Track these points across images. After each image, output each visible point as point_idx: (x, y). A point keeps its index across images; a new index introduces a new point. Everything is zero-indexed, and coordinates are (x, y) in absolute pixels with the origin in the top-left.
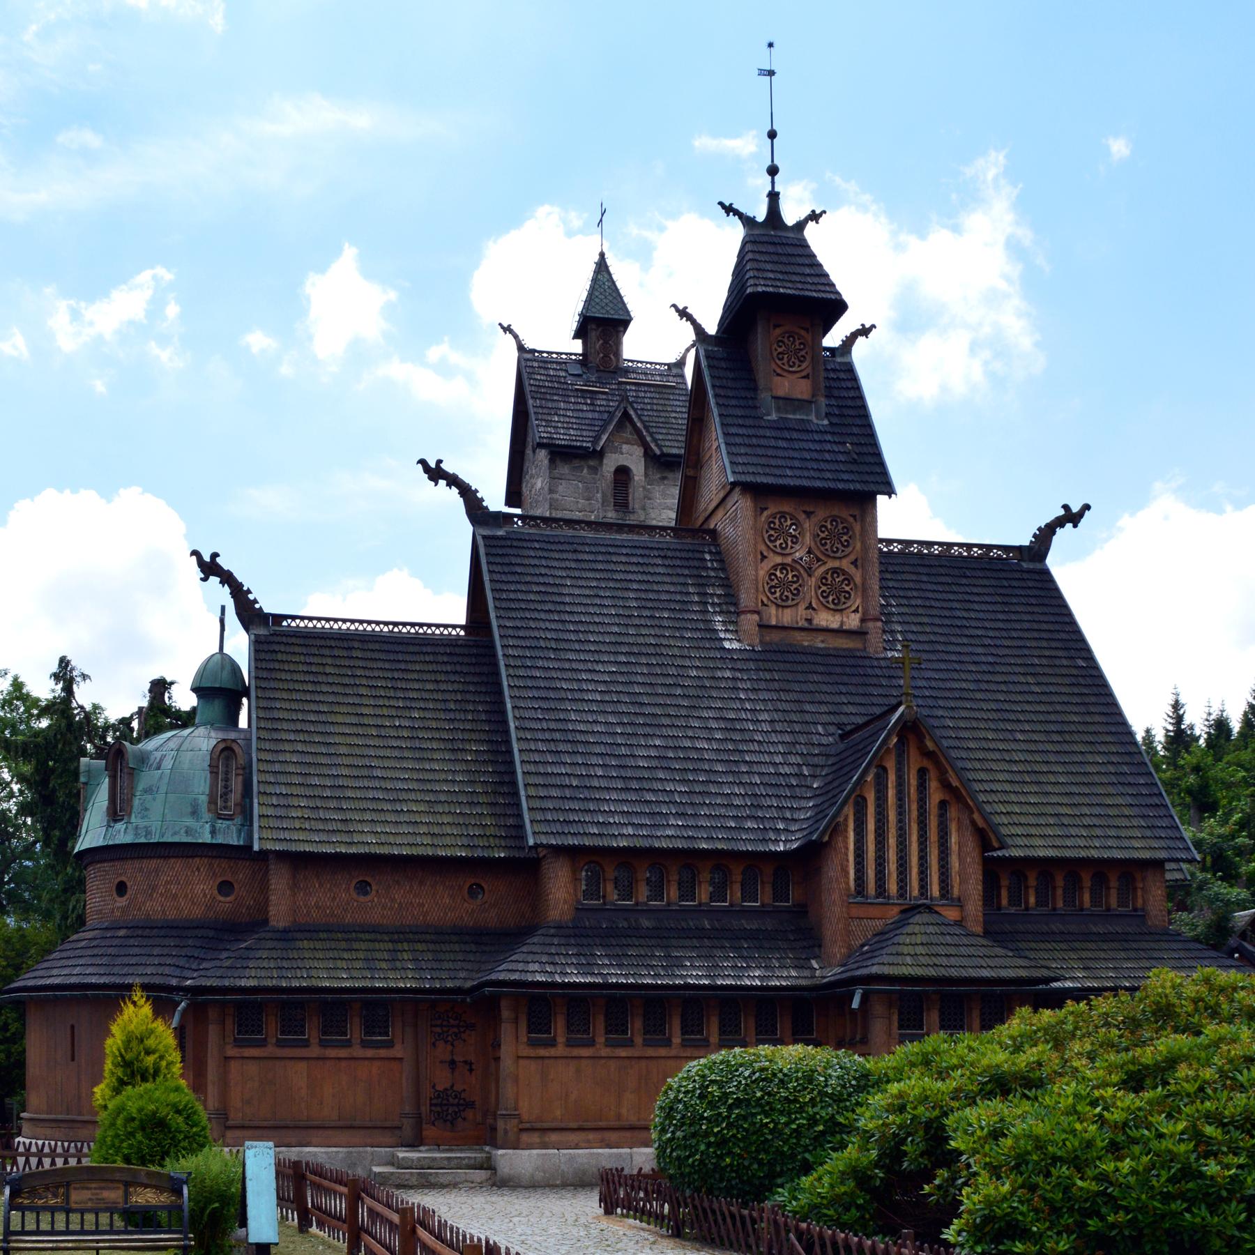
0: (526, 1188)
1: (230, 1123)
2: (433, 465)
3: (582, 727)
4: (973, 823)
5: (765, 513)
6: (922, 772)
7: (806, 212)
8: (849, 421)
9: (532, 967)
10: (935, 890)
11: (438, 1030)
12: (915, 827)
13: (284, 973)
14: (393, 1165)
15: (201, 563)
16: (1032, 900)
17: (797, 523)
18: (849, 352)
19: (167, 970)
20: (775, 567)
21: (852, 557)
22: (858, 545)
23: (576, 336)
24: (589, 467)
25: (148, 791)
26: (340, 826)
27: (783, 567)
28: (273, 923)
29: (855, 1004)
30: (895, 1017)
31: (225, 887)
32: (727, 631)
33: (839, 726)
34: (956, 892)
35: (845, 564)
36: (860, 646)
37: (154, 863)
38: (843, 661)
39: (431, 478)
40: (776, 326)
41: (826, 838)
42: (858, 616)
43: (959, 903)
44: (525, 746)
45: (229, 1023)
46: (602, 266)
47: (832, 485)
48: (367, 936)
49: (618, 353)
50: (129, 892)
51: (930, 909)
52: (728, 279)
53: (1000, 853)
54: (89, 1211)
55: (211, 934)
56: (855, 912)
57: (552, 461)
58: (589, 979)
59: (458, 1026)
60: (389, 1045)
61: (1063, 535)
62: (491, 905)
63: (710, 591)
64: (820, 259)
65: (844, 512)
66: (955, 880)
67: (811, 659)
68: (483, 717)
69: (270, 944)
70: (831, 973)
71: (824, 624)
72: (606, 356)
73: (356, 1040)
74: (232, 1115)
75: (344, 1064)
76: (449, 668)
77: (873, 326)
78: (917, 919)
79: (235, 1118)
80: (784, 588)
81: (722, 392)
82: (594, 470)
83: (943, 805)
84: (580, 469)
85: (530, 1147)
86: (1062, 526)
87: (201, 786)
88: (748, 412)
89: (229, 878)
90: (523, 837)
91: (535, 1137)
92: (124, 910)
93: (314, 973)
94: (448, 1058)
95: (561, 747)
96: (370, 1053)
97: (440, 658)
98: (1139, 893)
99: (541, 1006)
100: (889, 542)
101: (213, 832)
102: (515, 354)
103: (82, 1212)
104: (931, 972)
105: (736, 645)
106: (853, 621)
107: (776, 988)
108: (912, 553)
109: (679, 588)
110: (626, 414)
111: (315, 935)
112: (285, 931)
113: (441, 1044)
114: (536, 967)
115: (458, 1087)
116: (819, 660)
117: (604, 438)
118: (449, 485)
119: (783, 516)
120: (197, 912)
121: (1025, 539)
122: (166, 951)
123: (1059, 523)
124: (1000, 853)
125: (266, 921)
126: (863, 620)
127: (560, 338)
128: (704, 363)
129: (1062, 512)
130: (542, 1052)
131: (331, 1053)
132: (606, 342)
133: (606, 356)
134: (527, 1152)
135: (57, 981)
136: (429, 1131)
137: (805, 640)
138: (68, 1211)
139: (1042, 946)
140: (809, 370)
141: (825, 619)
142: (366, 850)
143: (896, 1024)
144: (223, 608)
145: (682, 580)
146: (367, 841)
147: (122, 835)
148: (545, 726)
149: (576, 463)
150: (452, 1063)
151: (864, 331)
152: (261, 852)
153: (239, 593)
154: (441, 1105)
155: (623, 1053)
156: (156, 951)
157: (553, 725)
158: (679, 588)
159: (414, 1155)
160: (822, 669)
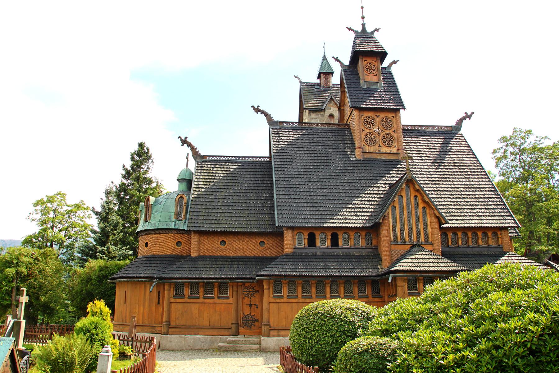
1: (170, 326)
3: (299, 186)
4: (435, 214)
6: (416, 197)
9: (274, 269)
10: (423, 239)
11: (246, 293)
12: (414, 217)
15: (182, 140)
16: (460, 243)
19: (154, 272)
21: (393, 130)
22: (395, 126)
26: (216, 222)
27: (370, 133)
29: (390, 280)
30: (406, 286)
31: (179, 243)
33: (389, 184)
34: (430, 240)
36: (397, 158)
41: (381, 221)
43: (432, 244)
44: (278, 193)
45: (172, 289)
48: (223, 260)
53: (447, 225)
55: (172, 259)
56: (393, 247)
58: (295, 274)
59: (253, 292)
60: (228, 298)
61: (466, 122)
62: (267, 248)
63: (347, 142)
65: (390, 115)
66: (430, 235)
67: (380, 163)
71: (385, 151)
73: (285, 296)
74: (172, 323)
75: (211, 305)
76: (259, 170)
79: (173, 324)
80: (370, 140)
81: (348, 81)
82: (322, 115)
83: (424, 208)
84: (318, 115)
85: (274, 336)
86: (465, 119)
87: (172, 210)
88: (356, 86)
90: (275, 225)
91: (275, 333)
92: (147, 251)
93: (201, 272)
95: (291, 193)
96: (221, 301)
97: (257, 167)
98: (500, 239)
99: (277, 282)
101: (175, 225)
102: (299, 84)
105: (354, 159)
106: (395, 150)
109: (336, 142)
110: (331, 98)
111: (205, 259)
113: (246, 298)
114: (276, 269)
115: (253, 314)
116: (383, 163)
117: (325, 105)
119: (369, 117)
120: (169, 253)
121: (453, 124)
122: (156, 265)
123: (464, 118)
124: (447, 225)
126: (398, 150)
127: (313, 78)
128: (343, 73)
129: (465, 115)
130: (278, 301)
131: (207, 301)
135: (120, 276)
136: (241, 330)
137: (378, 157)
139: (464, 259)
140: (377, 73)
141: (385, 149)
144: (188, 154)
145: (337, 139)
146: (224, 226)
147: (147, 227)
148: (286, 186)
149: (317, 113)
151: (395, 62)
152: (187, 230)
153: (193, 149)
154: (246, 320)
156: (153, 265)
157: (289, 186)
158: (336, 142)
160: (384, 166)
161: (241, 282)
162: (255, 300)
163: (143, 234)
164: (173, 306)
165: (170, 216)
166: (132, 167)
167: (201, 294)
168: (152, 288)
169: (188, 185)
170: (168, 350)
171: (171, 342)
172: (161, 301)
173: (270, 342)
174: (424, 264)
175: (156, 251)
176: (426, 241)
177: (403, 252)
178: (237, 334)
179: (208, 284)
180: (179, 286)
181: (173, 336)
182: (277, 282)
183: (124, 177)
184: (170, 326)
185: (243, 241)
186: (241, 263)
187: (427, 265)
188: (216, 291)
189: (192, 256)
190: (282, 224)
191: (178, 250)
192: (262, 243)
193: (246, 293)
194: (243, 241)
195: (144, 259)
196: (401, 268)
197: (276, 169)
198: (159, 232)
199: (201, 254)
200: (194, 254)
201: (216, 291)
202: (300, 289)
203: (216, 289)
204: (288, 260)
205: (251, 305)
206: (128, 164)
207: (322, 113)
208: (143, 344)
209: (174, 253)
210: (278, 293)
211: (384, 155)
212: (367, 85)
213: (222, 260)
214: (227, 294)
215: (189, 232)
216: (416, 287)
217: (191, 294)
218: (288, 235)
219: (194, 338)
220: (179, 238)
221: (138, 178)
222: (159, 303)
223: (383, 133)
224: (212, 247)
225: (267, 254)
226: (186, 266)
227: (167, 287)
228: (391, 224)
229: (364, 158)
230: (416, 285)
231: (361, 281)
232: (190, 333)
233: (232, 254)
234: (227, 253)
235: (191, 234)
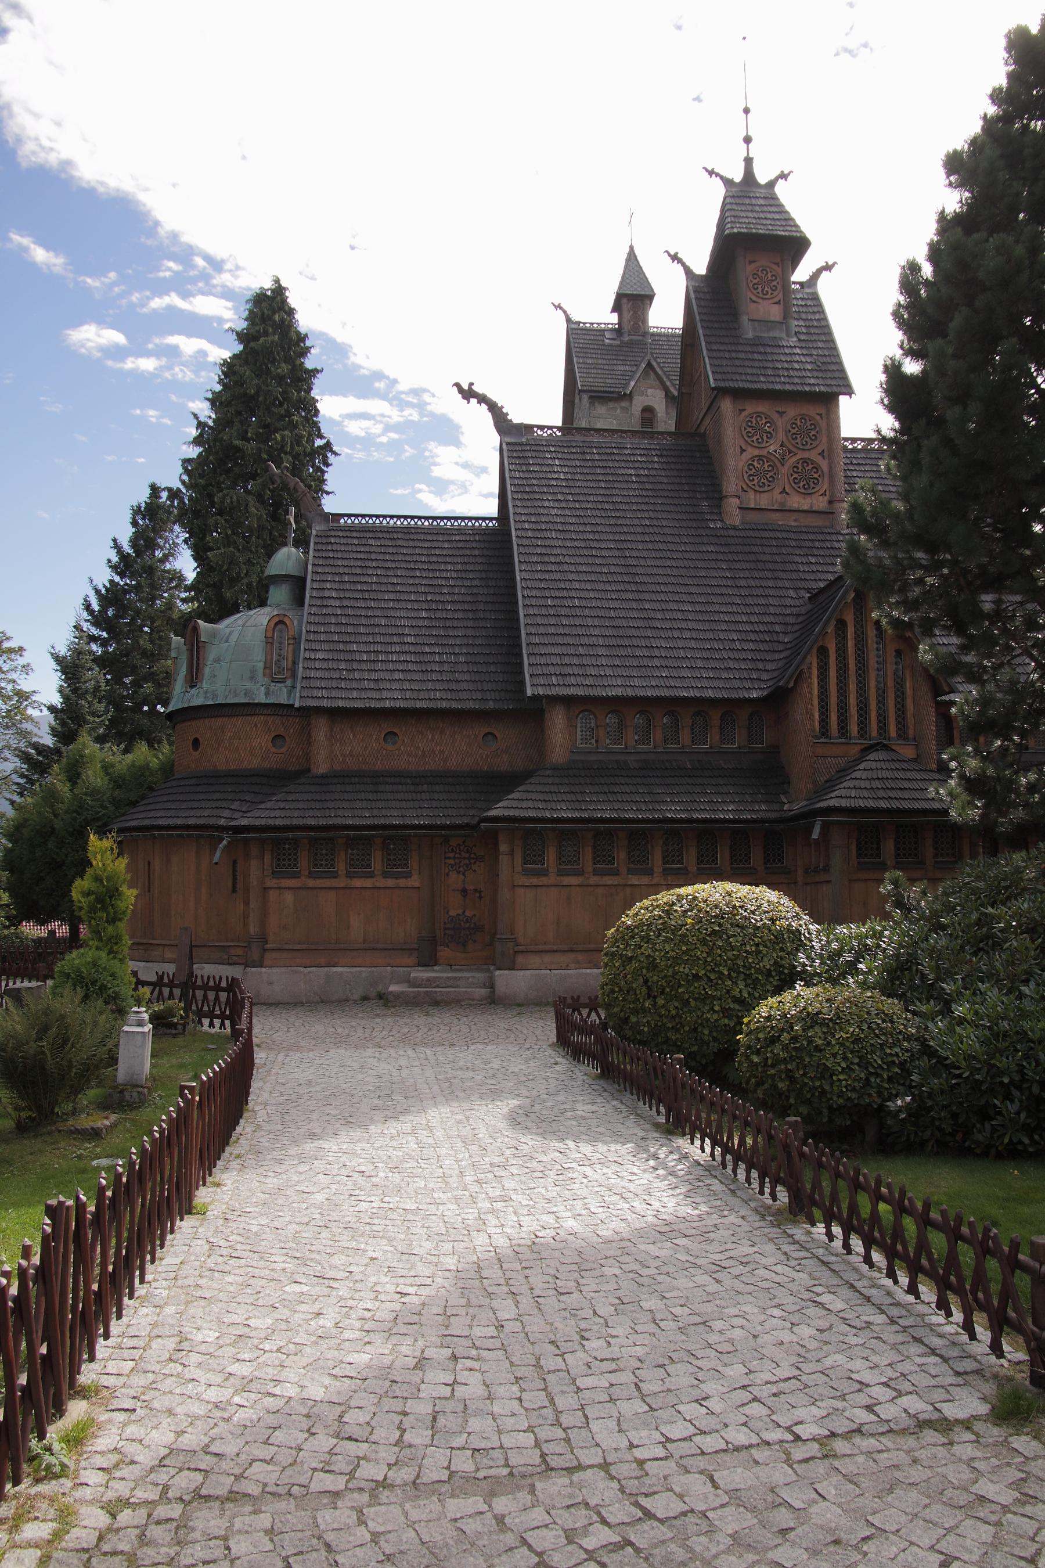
1: (268, 946)
2: (466, 387)
5: (744, 414)
7: (777, 173)
8: (815, 337)
10: (893, 733)
11: (452, 862)
17: (771, 422)
18: (815, 284)
20: (753, 459)
22: (825, 439)
23: (613, 311)
24: (622, 408)
25: (217, 660)
27: (760, 458)
28: (314, 771)
30: (854, 847)
32: (712, 513)
33: (808, 590)
34: (911, 733)
35: (813, 455)
37: (220, 721)
38: (813, 537)
39: (464, 398)
40: (751, 262)
42: (826, 498)
46: (632, 258)
47: (800, 388)
48: (392, 780)
49: (645, 321)
50: (201, 747)
51: (886, 748)
52: (714, 230)
57: (592, 404)
58: (577, 815)
59: (469, 858)
60: (408, 875)
62: (503, 749)
64: (788, 208)
65: (812, 410)
70: (797, 807)
71: (796, 506)
72: (636, 323)
77: (835, 263)
78: (871, 757)
80: (762, 473)
82: (625, 410)
89: (281, 731)
90: (524, 691)
96: (390, 882)
99: (532, 833)
100: (854, 440)
101: (267, 694)
104: (883, 804)
106: (820, 503)
107: (747, 821)
108: (873, 450)
112: (323, 776)
113: (453, 875)
117: (632, 383)
118: (479, 402)
119: (759, 415)
120: (255, 763)
125: (309, 770)
126: (830, 502)
128: (693, 296)
130: (535, 881)
131: (357, 883)
132: (635, 313)
133: (636, 323)
134: (522, 973)
136: (444, 953)
141: (796, 501)
142: (393, 704)
143: (854, 852)
146: (393, 698)
149: (611, 405)
150: (464, 892)
151: (828, 267)
152: (301, 708)
155: (609, 880)
161: (435, 838)
164: (272, 895)
166: (134, 542)
167: (341, 866)
168: (218, 853)
170: (264, 1004)
171: (270, 983)
172: (240, 885)
173: (513, 981)
174: (900, 794)
176: (899, 736)
177: (842, 762)
178: (428, 961)
181: (275, 970)
183: (114, 568)
184: (268, 946)
187: (906, 795)
188: (377, 862)
190: (541, 691)
192: (490, 737)
193: (452, 862)
195: (192, 781)
196: (844, 803)
197: (522, 550)
199: (337, 767)
200: (321, 767)
202: (588, 854)
203: (379, 853)
204: (557, 780)
205: (464, 892)
206: (125, 534)
207: (624, 404)
208: (211, 995)
209: (266, 765)
210: (534, 863)
211: (795, 516)
212: (754, 329)
213: (389, 780)
214: (406, 865)
215: (307, 713)
216: (878, 849)
217: (315, 865)
218: (557, 721)
221: (150, 570)
222: (234, 890)
223: (794, 459)
228: (816, 692)
229: (742, 523)
230: (878, 843)
231: (738, 833)
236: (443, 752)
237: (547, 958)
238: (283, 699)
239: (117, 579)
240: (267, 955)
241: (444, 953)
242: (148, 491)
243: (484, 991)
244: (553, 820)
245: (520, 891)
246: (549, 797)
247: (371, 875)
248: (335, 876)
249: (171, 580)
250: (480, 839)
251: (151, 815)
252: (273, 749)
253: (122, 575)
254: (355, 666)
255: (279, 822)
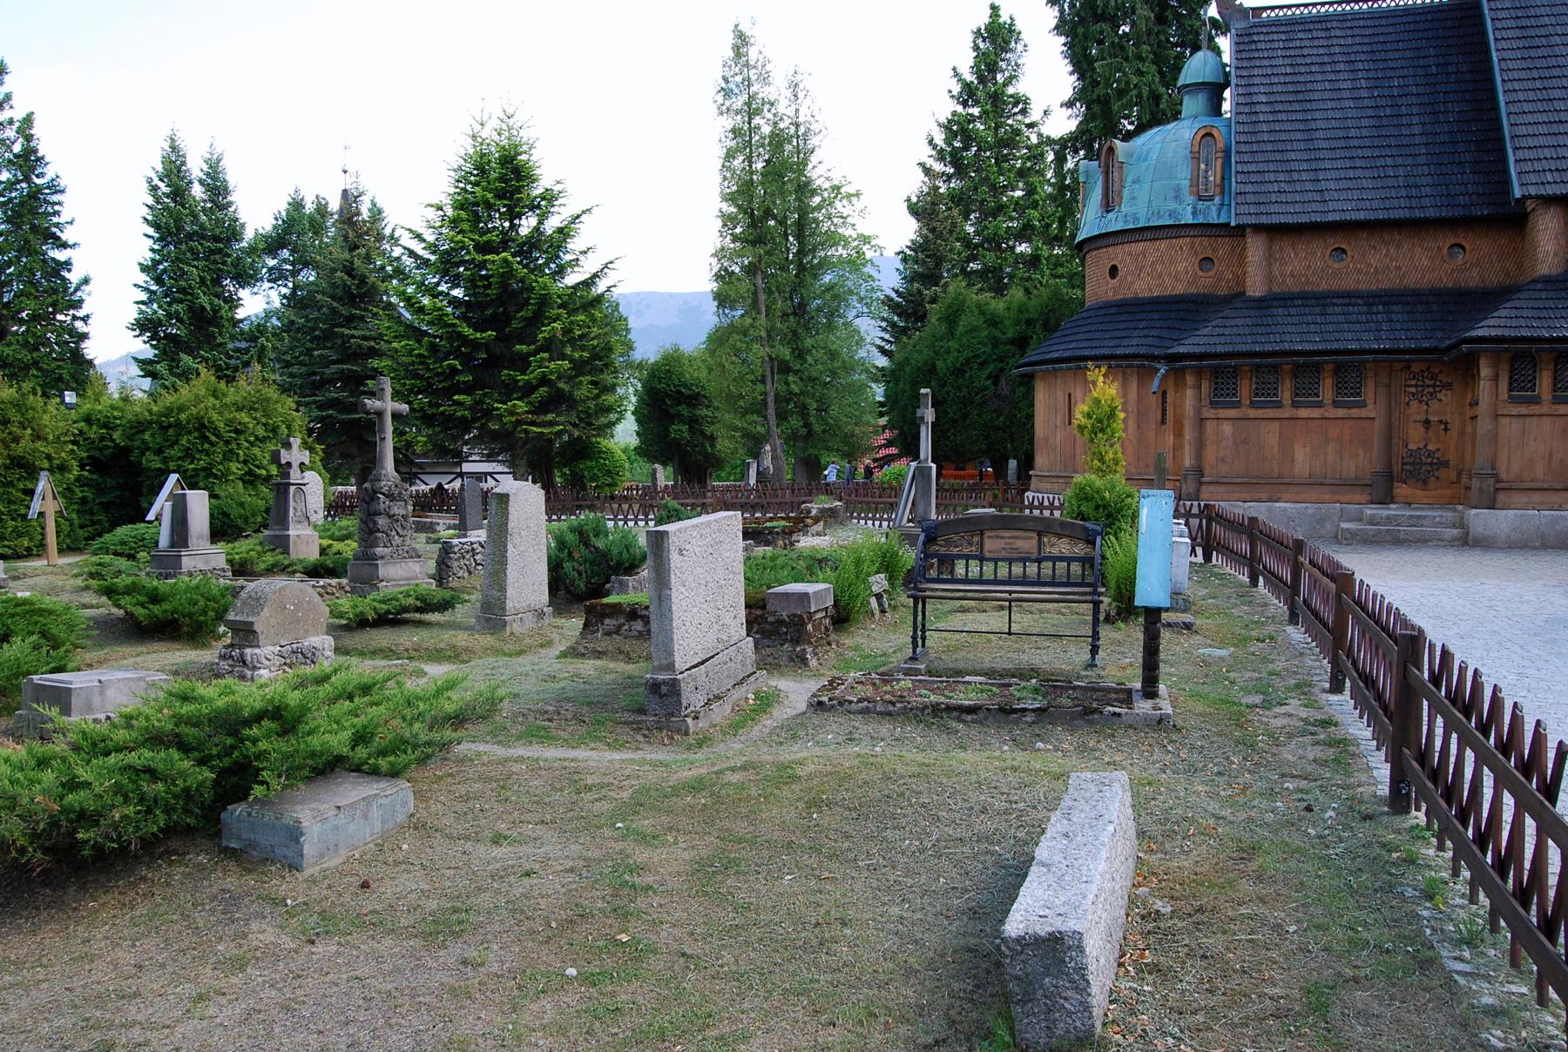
0: (1553, 548)
13: (1259, 338)
14: (1360, 520)
25: (1136, 181)
48: (1341, 301)
54: (1062, 559)
59: (1434, 386)
60: (1363, 405)
68: (1468, 76)
69: (1245, 312)
74: (1207, 471)
75: (1315, 423)
87: (1183, 177)
94: (1422, 417)
96: (1341, 412)
101: (1194, 213)
103: (996, 561)
112: (1260, 300)
113: (1414, 404)
120: (1180, 289)
130: (1523, 410)
131: (1304, 413)
135: (1056, 355)
136: (1401, 490)
138: (982, 559)
147: (1114, 223)
150: (1427, 422)
152: (1238, 226)
159: (1385, 513)
161: (1394, 360)
162: (1446, 404)
163: (1105, 242)
164: (1210, 425)
165: (1178, 190)
166: (976, 70)
167: (1286, 396)
169: (1210, 99)
175: (1142, 286)
178: (1387, 498)
179: (1304, 369)
180: (1221, 373)
182: (1521, 359)
185: (1398, 247)
186: (1395, 308)
188: (1327, 390)
189: (1250, 293)
190: (1533, 191)
191: (1204, 283)
192: (1207, 265)
194: (1398, 247)
195: (1113, 310)
197: (1498, 24)
198: (1149, 235)
199: (1276, 289)
200: (1255, 287)
201: (1327, 390)
203: (1288, 383)
204: (1551, 294)
205: (1427, 422)
206: (965, 61)
209: (1193, 290)
210: (1523, 389)
215: (1240, 231)
219: (1269, 510)
220: (1204, 245)
222: (1163, 422)
224: (1306, 266)
225: (1473, 279)
226: (1240, 322)
227: (1190, 380)
232: (1258, 496)
233: (1365, 284)
234: (1349, 284)
235: (1243, 236)
236: (1399, 268)
237: (1536, 497)
238: (1213, 218)
239: (960, 109)
240: (1204, 488)
241: (1401, 490)
242: (989, 12)
243: (1455, 532)
244: (1551, 340)
245: (1506, 421)
246: (1544, 314)
247: (1320, 405)
248: (1279, 405)
249: (1016, 104)
250: (1458, 364)
251: (1073, 345)
252: (1201, 273)
253: (965, 104)
254: (1295, 176)
255: (1219, 349)
